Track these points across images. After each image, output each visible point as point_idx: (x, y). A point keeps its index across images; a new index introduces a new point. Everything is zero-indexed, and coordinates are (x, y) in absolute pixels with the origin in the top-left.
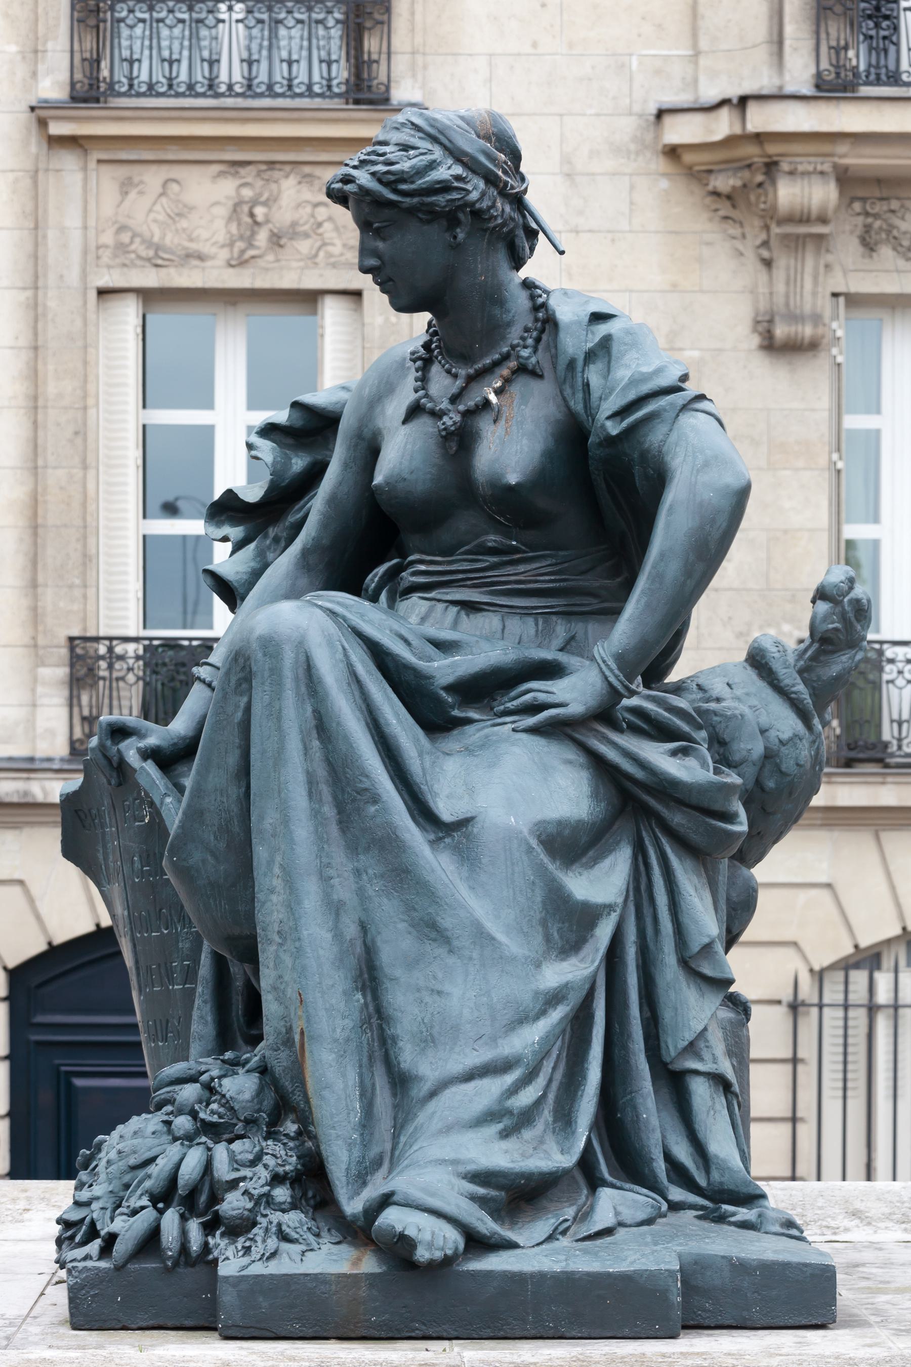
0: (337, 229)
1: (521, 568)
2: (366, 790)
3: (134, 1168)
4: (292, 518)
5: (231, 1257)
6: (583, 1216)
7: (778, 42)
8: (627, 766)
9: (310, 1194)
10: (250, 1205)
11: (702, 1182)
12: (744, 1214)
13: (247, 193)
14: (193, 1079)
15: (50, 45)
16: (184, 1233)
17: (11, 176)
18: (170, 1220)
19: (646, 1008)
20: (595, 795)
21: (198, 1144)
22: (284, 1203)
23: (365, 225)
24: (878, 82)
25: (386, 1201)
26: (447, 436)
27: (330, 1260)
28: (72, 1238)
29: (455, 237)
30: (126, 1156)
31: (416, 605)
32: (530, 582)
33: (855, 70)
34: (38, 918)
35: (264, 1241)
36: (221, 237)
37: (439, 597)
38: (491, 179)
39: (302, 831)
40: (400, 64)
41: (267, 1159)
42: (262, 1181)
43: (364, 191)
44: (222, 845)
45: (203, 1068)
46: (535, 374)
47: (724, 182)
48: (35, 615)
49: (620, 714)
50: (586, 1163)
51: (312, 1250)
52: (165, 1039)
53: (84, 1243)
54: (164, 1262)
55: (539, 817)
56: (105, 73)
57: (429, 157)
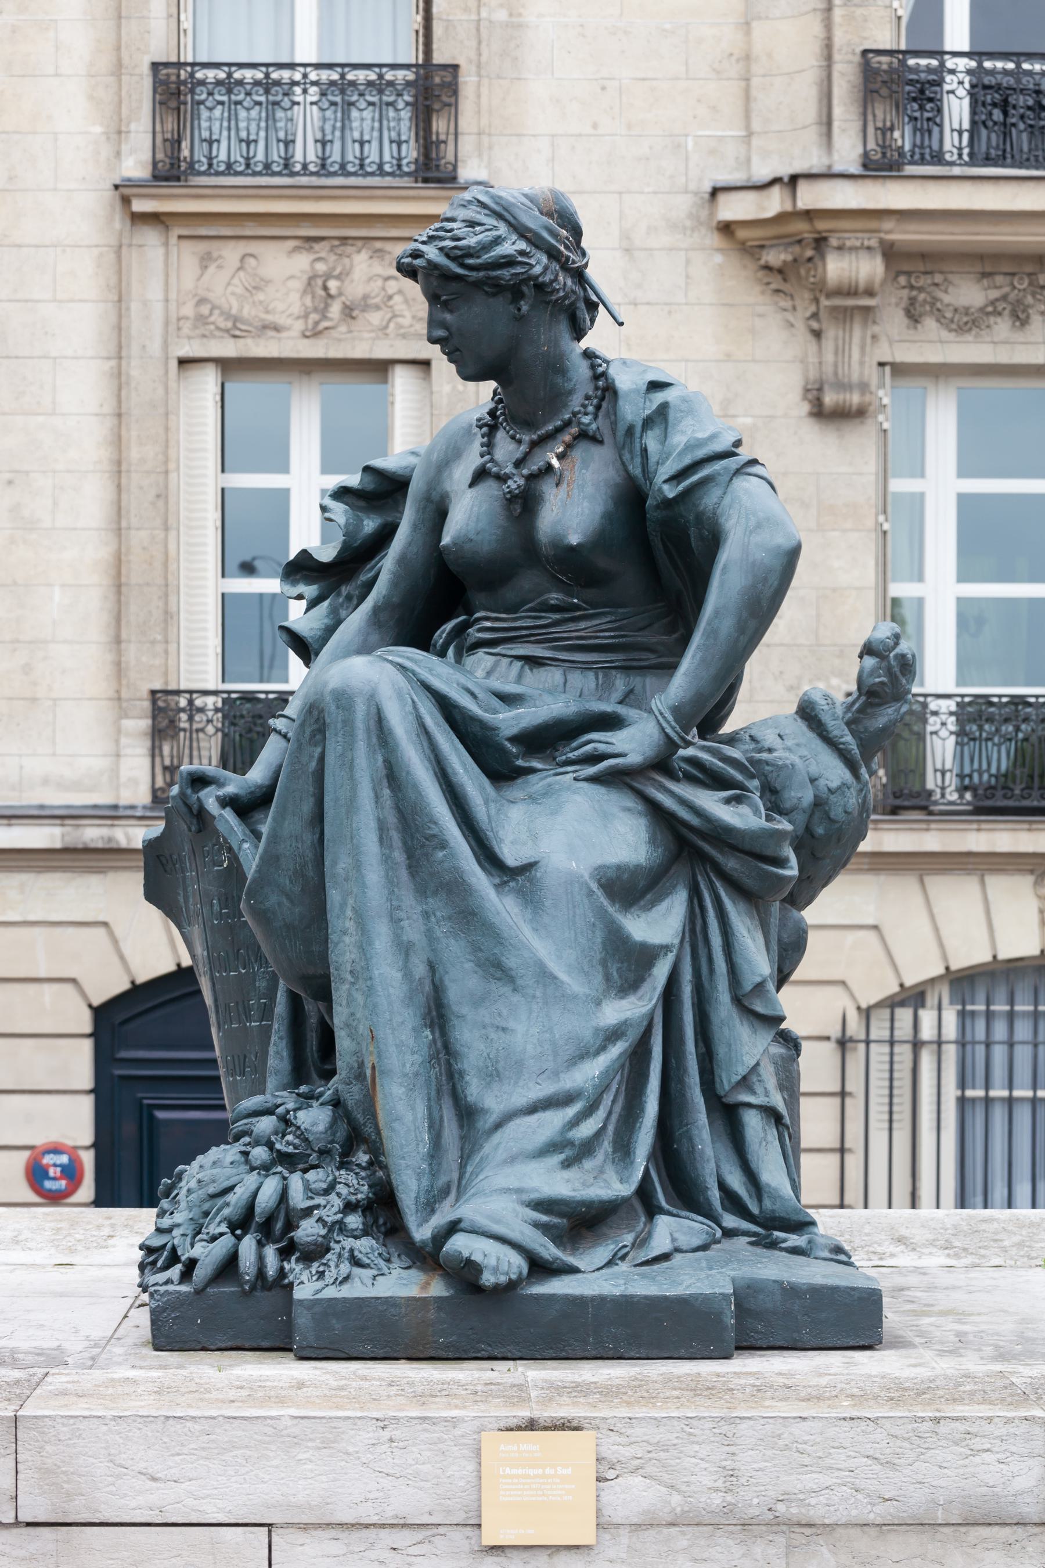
0: (406, 301)
1: (582, 625)
2: (434, 836)
3: (213, 1196)
4: (364, 577)
5: (306, 1281)
7: (827, 123)
9: (381, 1221)
10: (323, 1232)
11: (755, 1210)
12: (794, 1240)
13: (321, 267)
14: (269, 1112)
15: (133, 127)
16: (261, 1258)
17: (96, 251)
18: (248, 1246)
19: (701, 1044)
20: (652, 841)
21: (274, 1173)
22: (356, 1230)
23: (433, 298)
24: (922, 161)
25: (453, 1227)
26: (511, 499)
27: (399, 1283)
28: (154, 1263)
29: (519, 310)
30: (206, 1185)
31: (481, 661)
32: (591, 638)
33: (900, 150)
34: (122, 958)
35: (337, 1266)
36: (296, 309)
37: (504, 652)
38: (553, 254)
39: (374, 876)
40: (467, 145)
41: (341, 1188)
42: (335, 1209)
43: (432, 266)
44: (297, 889)
45: (279, 1101)
46: (596, 440)
47: (775, 257)
48: (119, 669)
49: (676, 764)
50: (644, 1192)
51: (382, 1275)
52: (243, 1073)
53: (166, 1267)
54: (241, 1285)
55: (599, 862)
56: (185, 152)
57: (495, 233)
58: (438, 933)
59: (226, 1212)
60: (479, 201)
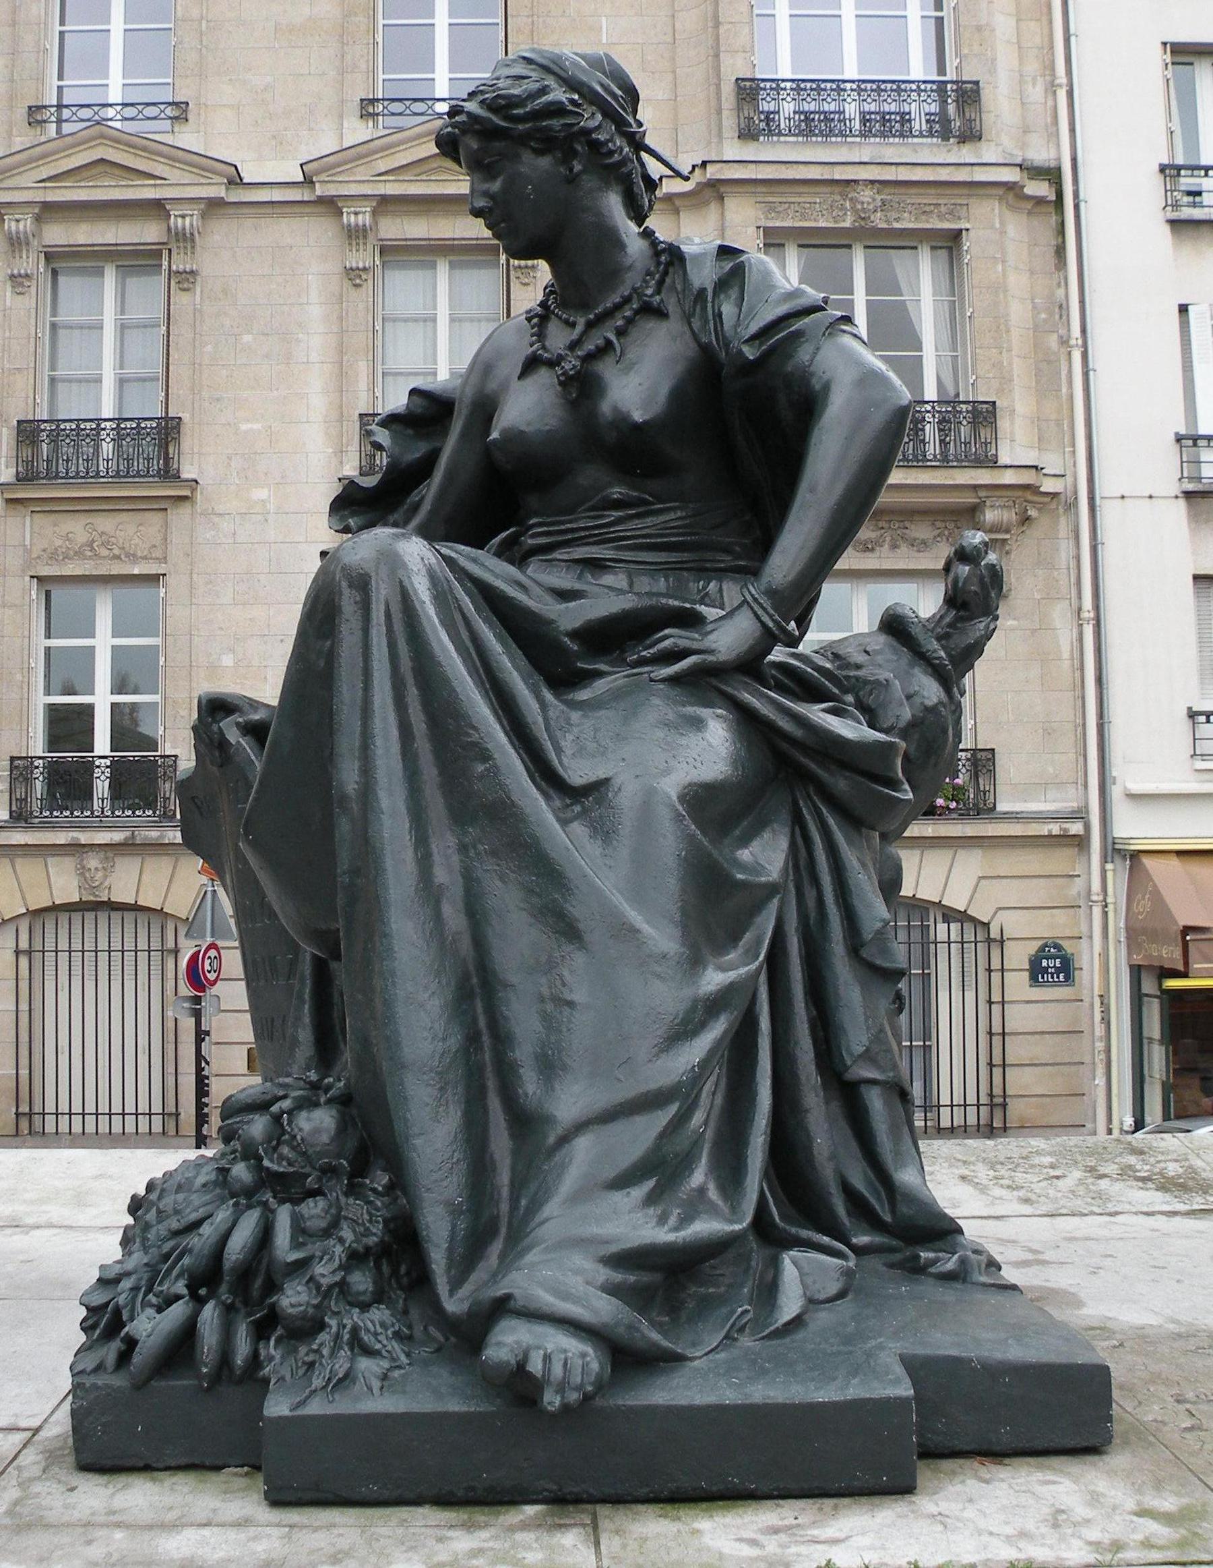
1: (649, 521)
2: (475, 744)
4: (414, 497)
6: (769, 1292)
8: (784, 723)
9: (403, 1269)
11: (888, 1218)
19: (812, 1008)
22: (365, 1292)
26: (566, 382)
29: (571, 170)
30: (168, 1217)
31: (535, 569)
38: (609, 114)
39: (391, 800)
41: (347, 1234)
46: (660, 313)
55: (688, 779)
58: (479, 873)
59: (186, 1261)
60: (524, 58)
